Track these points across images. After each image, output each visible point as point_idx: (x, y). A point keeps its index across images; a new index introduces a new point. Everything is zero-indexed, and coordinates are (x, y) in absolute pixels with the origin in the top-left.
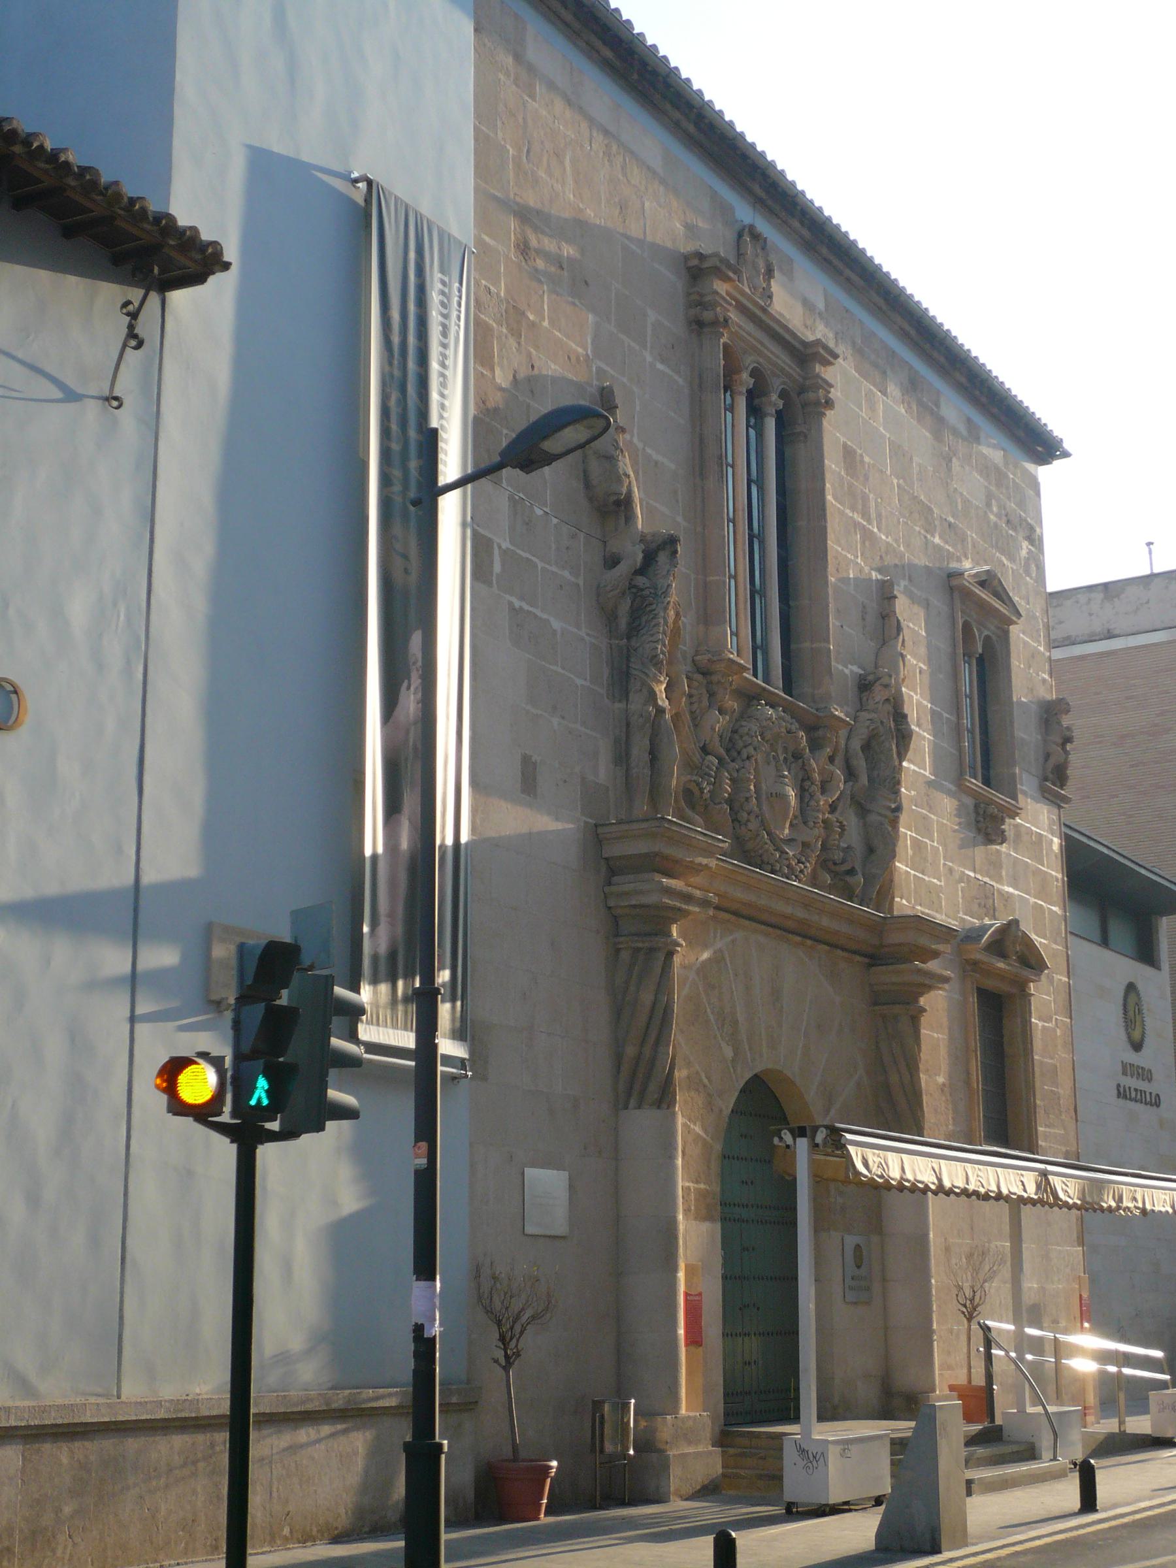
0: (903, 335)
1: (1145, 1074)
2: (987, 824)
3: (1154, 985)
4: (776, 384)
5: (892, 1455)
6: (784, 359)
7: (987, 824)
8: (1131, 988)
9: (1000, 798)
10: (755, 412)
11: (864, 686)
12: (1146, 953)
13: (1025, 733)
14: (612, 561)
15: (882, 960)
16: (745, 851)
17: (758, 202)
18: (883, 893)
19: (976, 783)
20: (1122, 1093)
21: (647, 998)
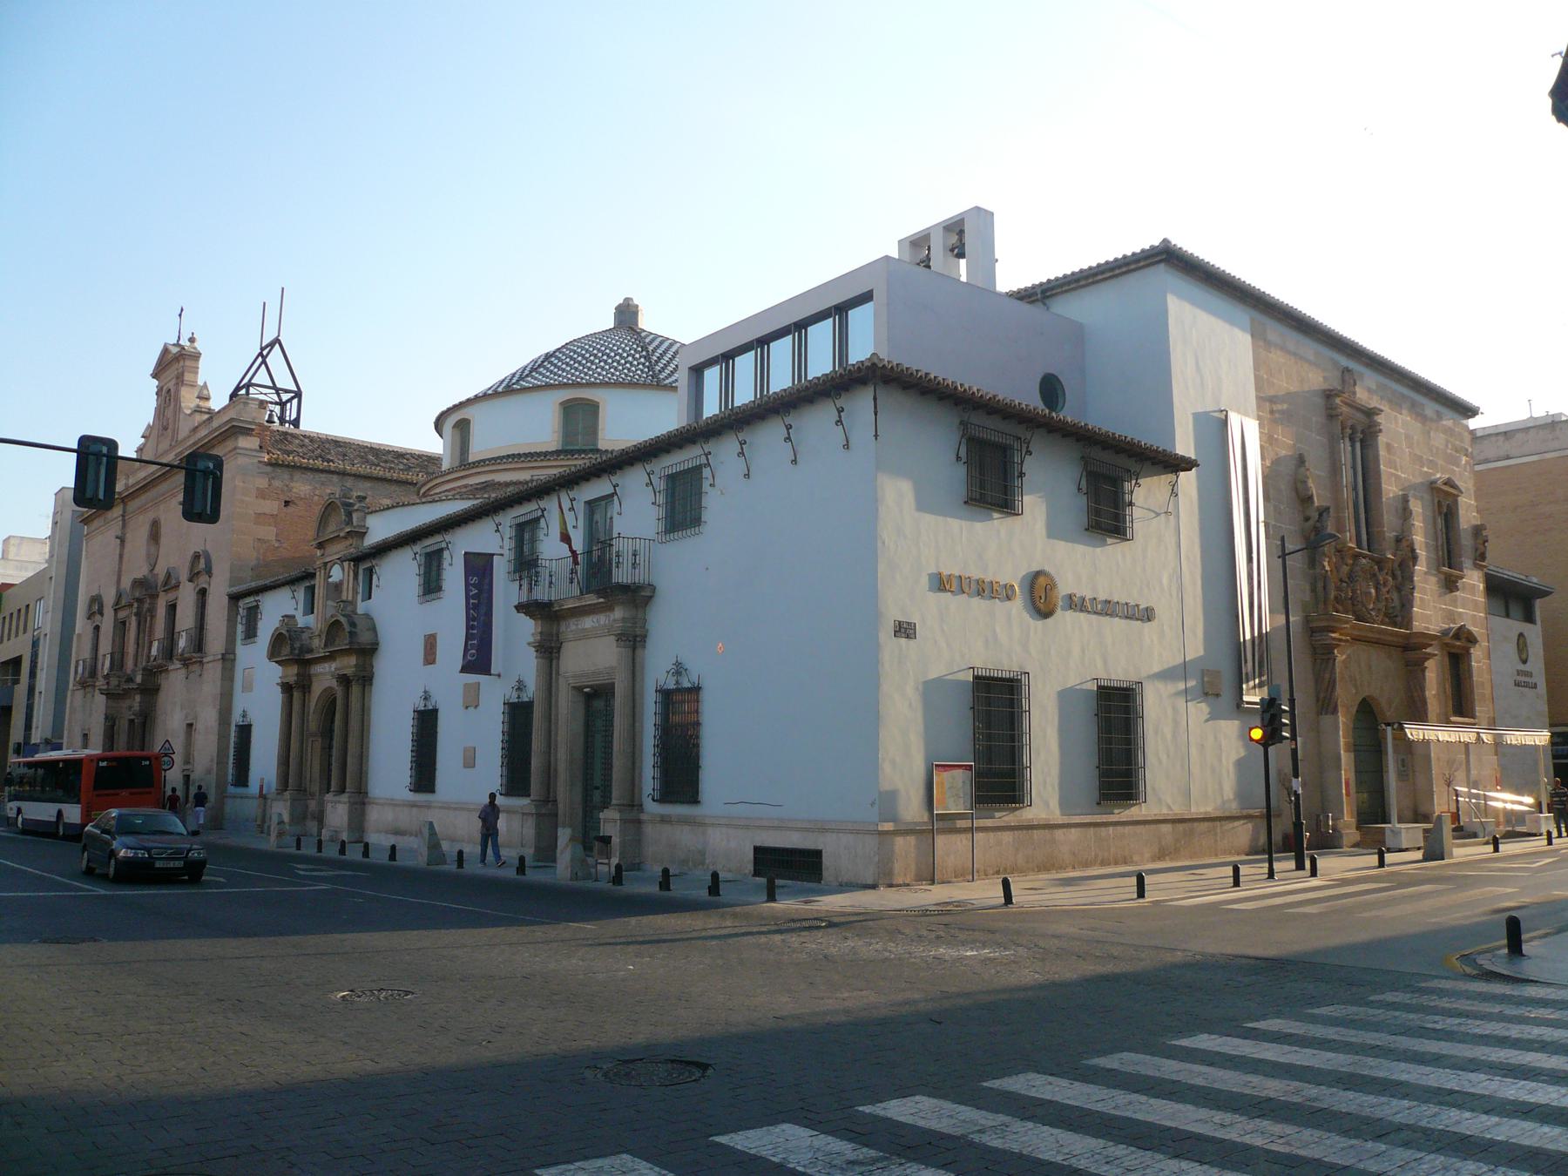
0: (1408, 386)
1: (1529, 674)
2: (1450, 584)
3: (1534, 633)
4: (1359, 428)
5: (1555, 757)
6: (1360, 416)
8: (1521, 635)
10: (1352, 440)
11: (1398, 540)
13: (1466, 541)
14: (1307, 519)
15: (1410, 650)
20: (1517, 684)
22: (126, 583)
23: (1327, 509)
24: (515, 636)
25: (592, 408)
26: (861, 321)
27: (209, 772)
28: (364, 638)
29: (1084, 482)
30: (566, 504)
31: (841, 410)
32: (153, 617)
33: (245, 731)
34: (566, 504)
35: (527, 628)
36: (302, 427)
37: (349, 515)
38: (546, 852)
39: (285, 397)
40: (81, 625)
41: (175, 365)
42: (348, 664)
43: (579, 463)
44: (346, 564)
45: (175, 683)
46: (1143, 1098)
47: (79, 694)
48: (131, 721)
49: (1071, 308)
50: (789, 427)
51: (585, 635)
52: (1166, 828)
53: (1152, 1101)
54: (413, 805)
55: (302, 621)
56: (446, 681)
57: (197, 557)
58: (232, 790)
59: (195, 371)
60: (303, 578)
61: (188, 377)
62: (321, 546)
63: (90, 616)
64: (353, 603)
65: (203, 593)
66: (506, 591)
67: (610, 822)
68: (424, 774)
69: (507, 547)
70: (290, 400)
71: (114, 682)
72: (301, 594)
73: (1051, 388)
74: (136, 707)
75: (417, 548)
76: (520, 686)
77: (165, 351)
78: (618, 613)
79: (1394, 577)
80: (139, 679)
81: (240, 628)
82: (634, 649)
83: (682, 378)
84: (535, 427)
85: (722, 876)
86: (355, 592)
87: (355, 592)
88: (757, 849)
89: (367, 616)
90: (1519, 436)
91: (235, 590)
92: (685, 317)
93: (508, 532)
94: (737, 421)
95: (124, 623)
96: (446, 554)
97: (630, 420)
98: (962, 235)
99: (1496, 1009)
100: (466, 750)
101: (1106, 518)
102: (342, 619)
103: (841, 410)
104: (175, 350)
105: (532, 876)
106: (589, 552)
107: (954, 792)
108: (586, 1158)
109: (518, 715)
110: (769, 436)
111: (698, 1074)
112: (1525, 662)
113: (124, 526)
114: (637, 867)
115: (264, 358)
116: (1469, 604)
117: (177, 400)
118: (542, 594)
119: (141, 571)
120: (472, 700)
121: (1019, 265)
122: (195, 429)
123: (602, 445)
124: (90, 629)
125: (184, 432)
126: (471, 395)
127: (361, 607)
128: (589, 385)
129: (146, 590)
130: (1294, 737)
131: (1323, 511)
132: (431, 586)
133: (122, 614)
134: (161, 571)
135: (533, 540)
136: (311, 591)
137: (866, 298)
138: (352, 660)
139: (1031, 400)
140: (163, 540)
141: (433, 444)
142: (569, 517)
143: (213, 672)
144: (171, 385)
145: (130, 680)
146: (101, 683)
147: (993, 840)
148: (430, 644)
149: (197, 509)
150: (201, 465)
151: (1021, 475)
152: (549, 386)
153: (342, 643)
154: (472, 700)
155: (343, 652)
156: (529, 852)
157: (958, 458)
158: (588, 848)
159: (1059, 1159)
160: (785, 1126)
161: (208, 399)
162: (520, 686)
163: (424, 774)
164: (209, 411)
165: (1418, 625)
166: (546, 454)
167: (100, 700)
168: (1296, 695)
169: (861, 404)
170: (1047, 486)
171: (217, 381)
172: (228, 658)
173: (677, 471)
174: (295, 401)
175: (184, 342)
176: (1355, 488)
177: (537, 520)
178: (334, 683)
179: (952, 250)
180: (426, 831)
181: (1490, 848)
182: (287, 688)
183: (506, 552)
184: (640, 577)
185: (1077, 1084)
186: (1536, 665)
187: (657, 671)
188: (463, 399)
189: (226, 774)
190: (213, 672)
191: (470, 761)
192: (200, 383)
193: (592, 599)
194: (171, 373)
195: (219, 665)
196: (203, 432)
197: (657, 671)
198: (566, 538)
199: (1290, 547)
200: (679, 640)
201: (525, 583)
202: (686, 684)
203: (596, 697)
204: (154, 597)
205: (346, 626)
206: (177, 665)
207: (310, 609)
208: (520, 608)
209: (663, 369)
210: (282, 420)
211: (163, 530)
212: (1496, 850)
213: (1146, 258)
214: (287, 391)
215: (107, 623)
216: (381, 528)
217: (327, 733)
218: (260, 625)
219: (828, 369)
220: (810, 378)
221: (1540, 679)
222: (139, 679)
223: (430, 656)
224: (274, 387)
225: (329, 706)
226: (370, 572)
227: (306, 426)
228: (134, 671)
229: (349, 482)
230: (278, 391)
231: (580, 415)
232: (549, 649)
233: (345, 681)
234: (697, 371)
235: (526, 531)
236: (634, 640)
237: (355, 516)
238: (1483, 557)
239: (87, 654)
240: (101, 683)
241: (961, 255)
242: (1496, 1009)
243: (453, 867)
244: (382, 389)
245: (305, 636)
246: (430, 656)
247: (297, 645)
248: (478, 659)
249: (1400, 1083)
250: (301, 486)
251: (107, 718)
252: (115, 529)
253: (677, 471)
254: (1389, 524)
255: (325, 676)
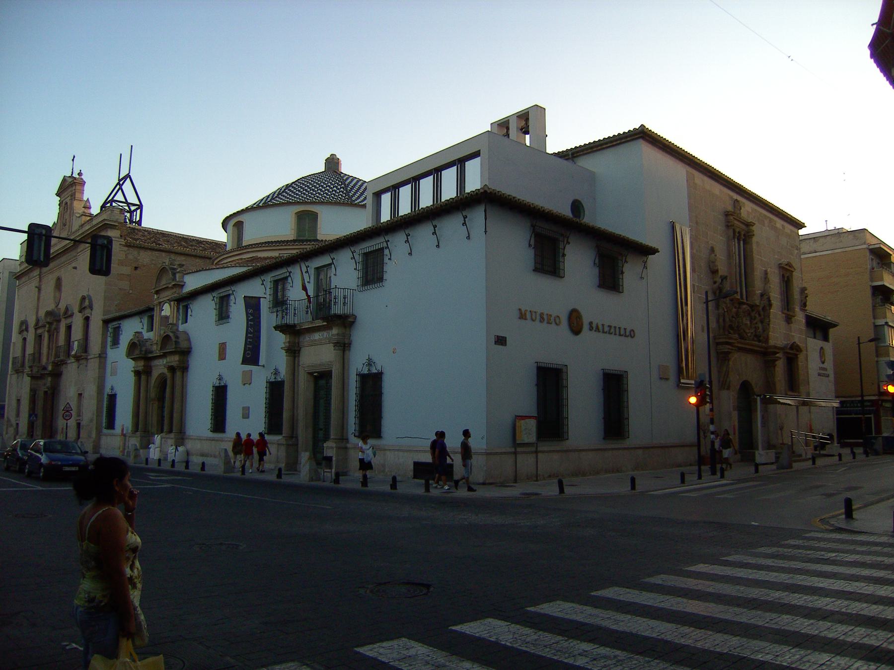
0: (767, 210)
1: (825, 369)
2: (789, 319)
3: (828, 347)
4: (743, 233)
5: (837, 414)
6: (743, 227)
7: (789, 319)
8: (822, 348)
9: (791, 314)
10: (739, 240)
11: (762, 295)
12: (826, 338)
13: (796, 295)
14: (715, 283)
15: (767, 355)
16: (742, 338)
17: (737, 193)
18: (767, 339)
19: (786, 311)
20: (819, 375)
21: (725, 369)
22: (42, 313)
23: (726, 277)
24: (273, 344)
25: (314, 216)
26: (473, 168)
27: (91, 421)
28: (183, 345)
29: (597, 261)
30: (304, 269)
31: (465, 217)
32: (58, 332)
33: (112, 398)
34: (304, 269)
35: (281, 339)
36: (143, 225)
37: (174, 274)
38: (293, 465)
39: (133, 208)
40: (15, 337)
41: (70, 188)
42: (174, 360)
43: (308, 247)
44: (172, 303)
45: (71, 371)
46: (685, 600)
47: (15, 377)
48: (46, 392)
49: (587, 163)
50: (435, 227)
51: (314, 343)
52: (640, 452)
53: (690, 601)
54: (213, 440)
55: (147, 335)
56: (233, 369)
57: (83, 298)
58: (105, 431)
59: (82, 192)
60: (147, 312)
61: (77, 195)
62: (157, 292)
63: (21, 332)
64: (176, 325)
65: (87, 319)
66: (268, 319)
67: (330, 449)
68: (219, 423)
69: (268, 293)
70: (136, 210)
71: (35, 370)
72: (145, 320)
73: (577, 207)
74: (49, 384)
75: (215, 294)
76: (276, 372)
77: (64, 180)
78: (335, 331)
79: (760, 315)
80: (50, 368)
81: (109, 339)
82: (344, 351)
83: (369, 202)
84: (281, 226)
85: (398, 478)
86: (178, 319)
87: (178, 319)
88: (416, 464)
89: (185, 333)
90: (821, 240)
91: (106, 317)
92: (366, 166)
93: (269, 285)
94: (400, 224)
95: (40, 336)
96: (232, 297)
97: (335, 224)
98: (528, 120)
99: (852, 547)
100: (244, 408)
101: (610, 281)
102: (171, 335)
103: (465, 217)
104: (70, 180)
105: (285, 479)
106: (317, 296)
107: (529, 431)
108: (382, 641)
109: (275, 389)
110: (423, 234)
111: (425, 591)
112: (823, 363)
113: (40, 281)
114: (345, 474)
115: (121, 186)
116: (798, 332)
117: (72, 208)
118: (290, 320)
119: (51, 307)
120: (247, 380)
121: (557, 141)
122: (82, 226)
123: (319, 237)
124: (21, 340)
125: (75, 227)
126: (244, 207)
127: (181, 328)
128: (312, 203)
129: (53, 319)
130: (711, 403)
131: (724, 278)
132: (223, 316)
133: (39, 331)
134: (62, 306)
135: (284, 289)
136: (151, 318)
137: (476, 154)
138: (176, 358)
139: (567, 212)
140: (63, 289)
141: (221, 236)
142: (306, 276)
143: (93, 364)
144: (68, 200)
145: (45, 368)
146: (27, 370)
147: (550, 459)
148: (223, 348)
149: (98, 267)
150: (100, 241)
151: (564, 255)
152: (289, 204)
153: (170, 348)
154: (247, 380)
155: (171, 353)
156: (282, 465)
157: (530, 245)
158: (319, 464)
159: (654, 635)
160: (490, 620)
161: (90, 208)
162: (276, 372)
163: (219, 423)
164: (91, 215)
165: (772, 342)
166: (288, 241)
167: (27, 380)
168: (713, 379)
169: (477, 216)
170: (578, 260)
171: (95, 196)
172: (102, 356)
173: (370, 250)
174: (139, 211)
175: (76, 175)
176: (740, 267)
177: (286, 278)
178: (165, 371)
179: (521, 129)
180: (223, 454)
181: (810, 462)
182: (137, 373)
183: (268, 296)
184: (347, 310)
185: (644, 593)
186: (829, 365)
187: (357, 363)
188: (239, 209)
189: (102, 423)
190: (93, 364)
191: (246, 415)
192: (85, 199)
193: (319, 323)
194: (67, 194)
195: (97, 360)
196: (87, 227)
197: (357, 363)
198: (304, 288)
199: (710, 299)
200: (369, 347)
201: (280, 314)
202: (374, 371)
203: (321, 378)
204: (59, 321)
205: (173, 339)
206: (73, 360)
207: (151, 328)
208: (276, 328)
209: (354, 195)
210: (131, 221)
211: (63, 284)
212: (814, 463)
213: (631, 136)
214: (134, 205)
215: (31, 336)
216: (193, 282)
217: (161, 399)
218: (121, 337)
219: (454, 195)
220: (443, 200)
221: (831, 372)
222: (50, 368)
223: (222, 355)
224: (126, 202)
225: (162, 383)
226: (186, 308)
227: (145, 224)
228: (46, 363)
229: (173, 256)
230: (129, 204)
231: (307, 220)
232: (293, 351)
233: (172, 369)
234: (378, 195)
235: (280, 285)
236: (344, 346)
237: (178, 276)
238: (805, 305)
239: (19, 353)
240: (27, 370)
241: (527, 133)
242: (852, 547)
243: (239, 475)
244: (190, 203)
245: (148, 343)
246: (222, 355)
247: (144, 349)
248: (251, 356)
249: (821, 588)
250: (145, 257)
251: (31, 390)
252: (35, 283)
253: (370, 250)
254: (758, 286)
255: (160, 367)
